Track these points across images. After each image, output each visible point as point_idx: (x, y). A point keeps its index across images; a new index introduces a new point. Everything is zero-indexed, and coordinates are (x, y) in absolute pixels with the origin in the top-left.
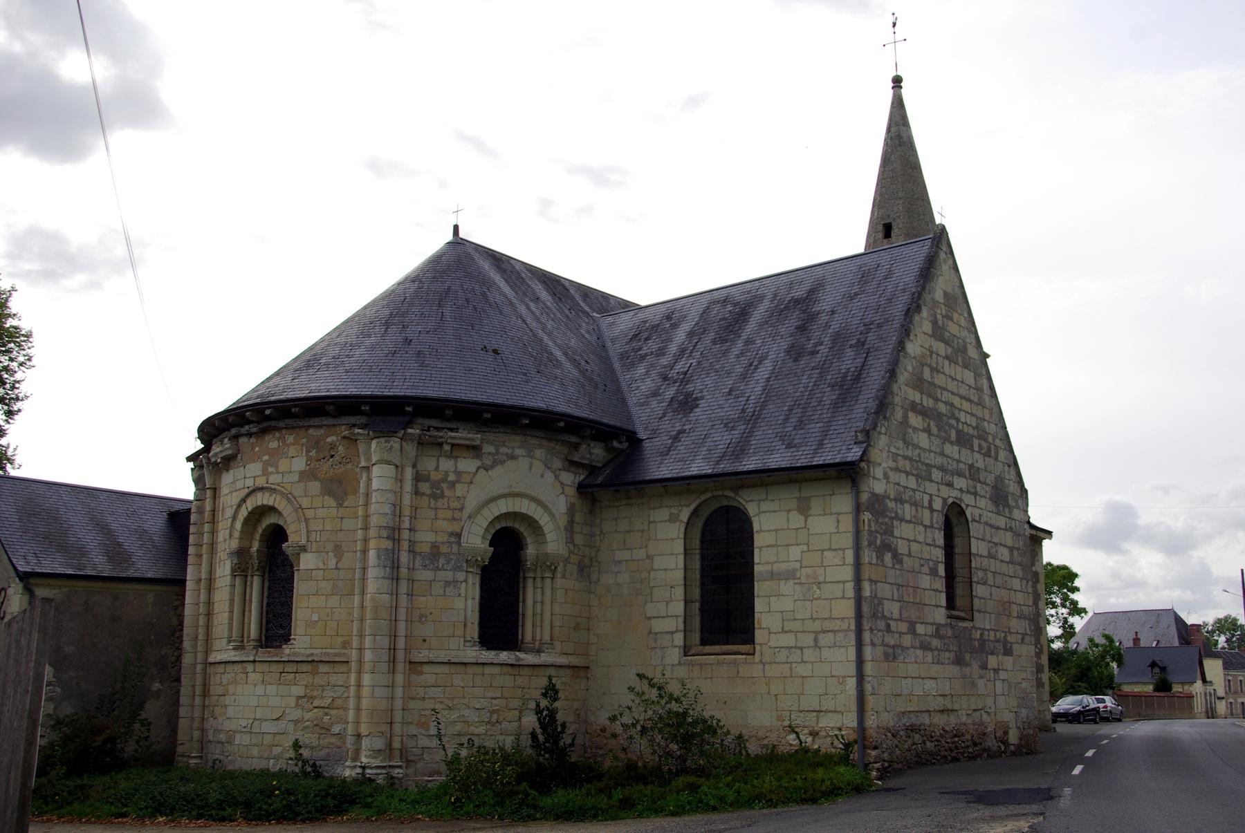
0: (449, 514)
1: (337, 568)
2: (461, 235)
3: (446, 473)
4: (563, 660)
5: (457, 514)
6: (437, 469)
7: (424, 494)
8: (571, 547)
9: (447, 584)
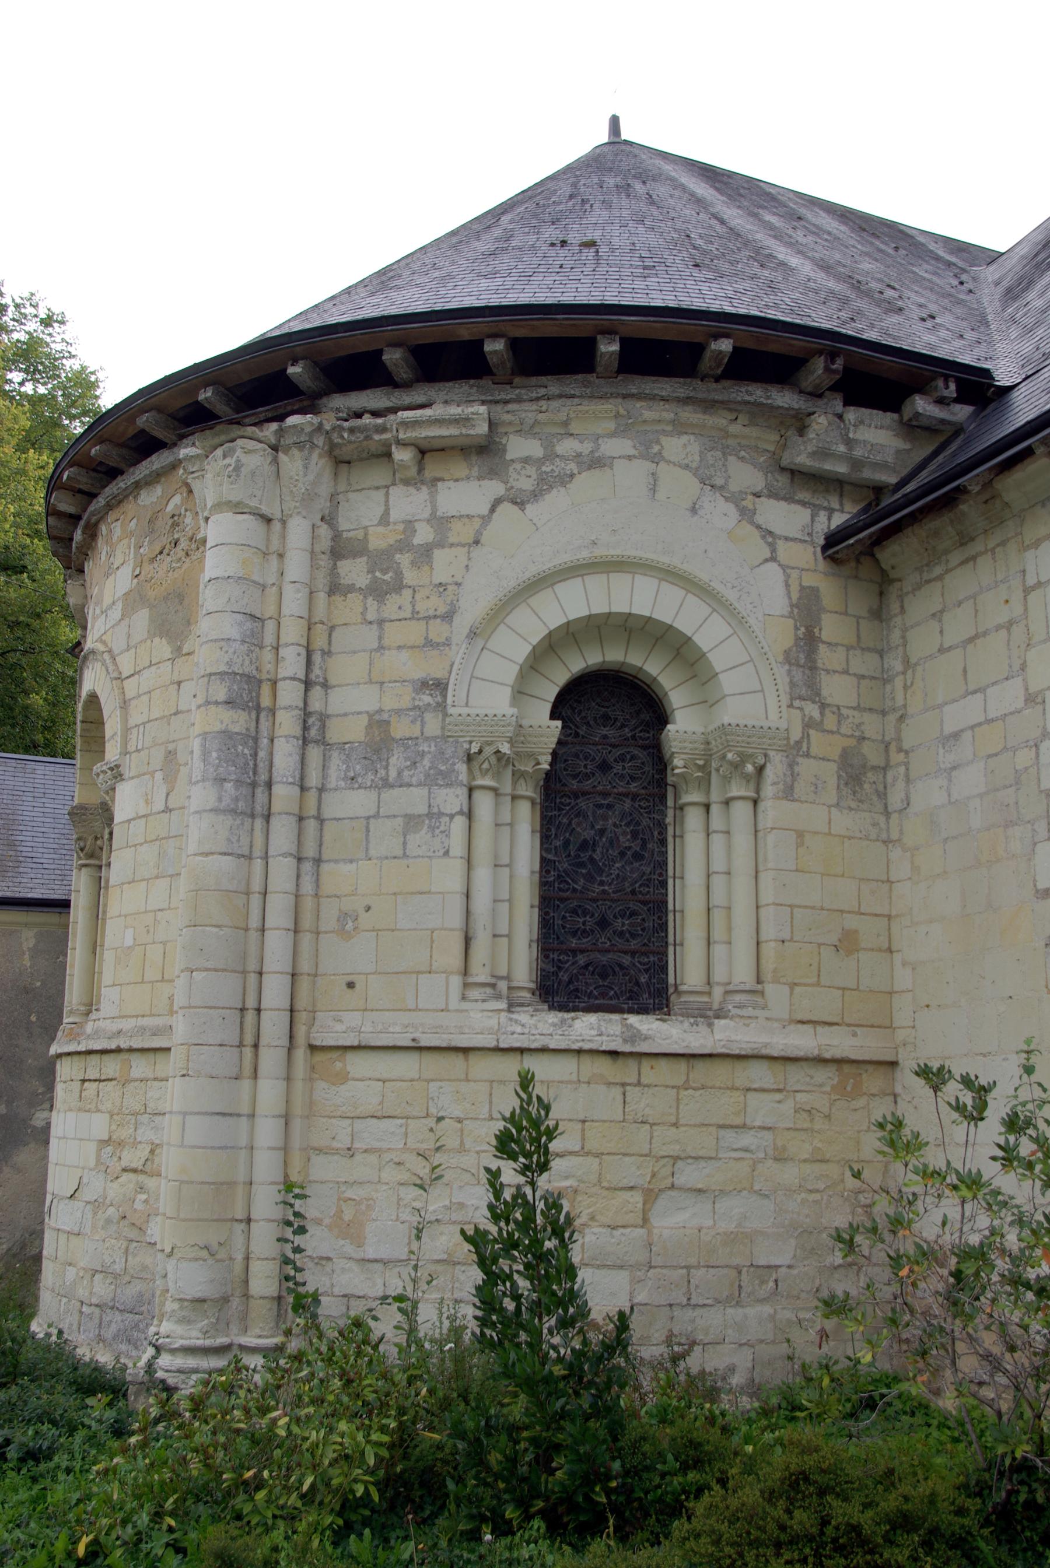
0: (415, 632)
1: (167, 810)
2: (625, 135)
3: (409, 525)
4: (801, 1041)
5: (438, 630)
6: (384, 520)
7: (351, 589)
8: (812, 710)
9: (412, 822)
